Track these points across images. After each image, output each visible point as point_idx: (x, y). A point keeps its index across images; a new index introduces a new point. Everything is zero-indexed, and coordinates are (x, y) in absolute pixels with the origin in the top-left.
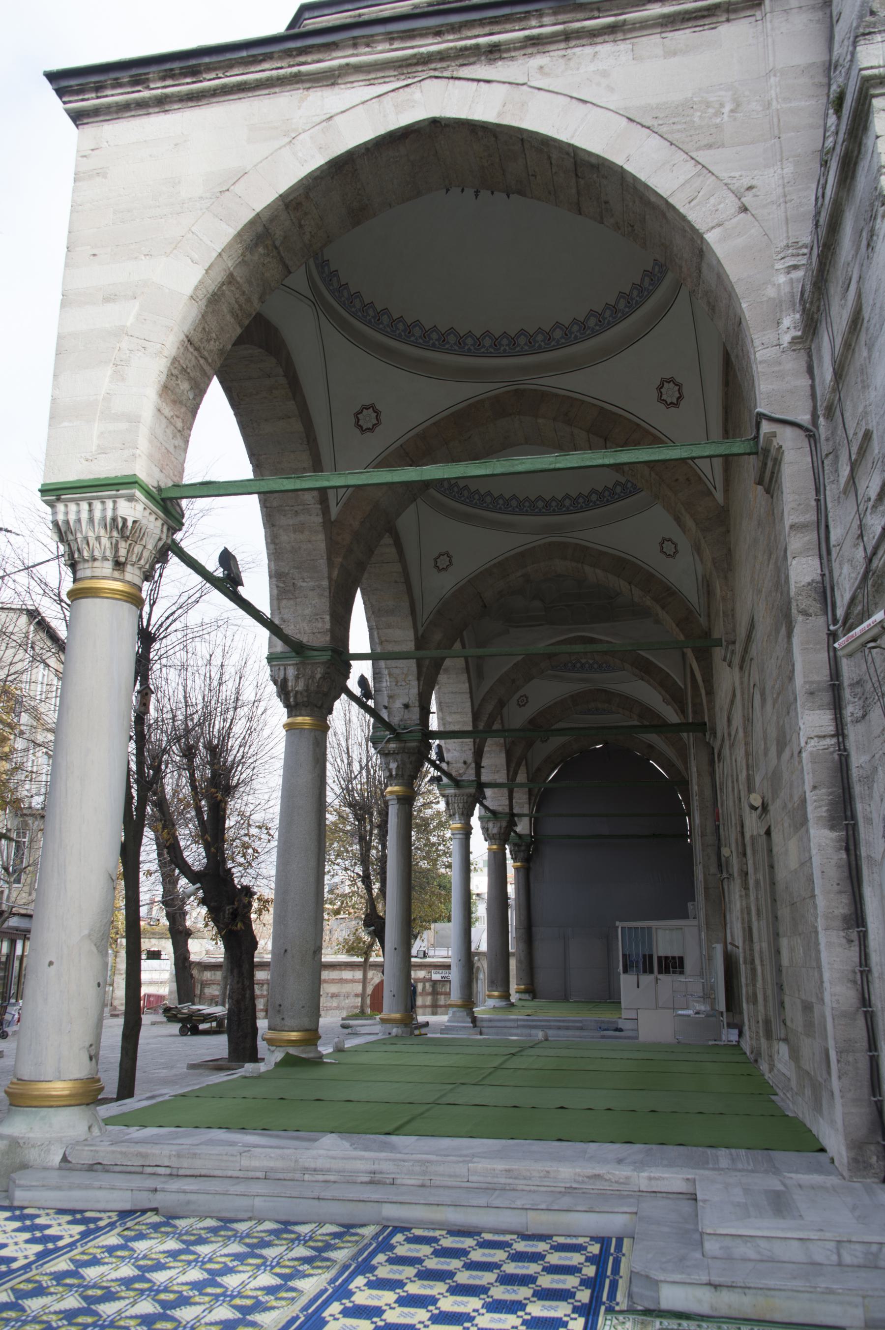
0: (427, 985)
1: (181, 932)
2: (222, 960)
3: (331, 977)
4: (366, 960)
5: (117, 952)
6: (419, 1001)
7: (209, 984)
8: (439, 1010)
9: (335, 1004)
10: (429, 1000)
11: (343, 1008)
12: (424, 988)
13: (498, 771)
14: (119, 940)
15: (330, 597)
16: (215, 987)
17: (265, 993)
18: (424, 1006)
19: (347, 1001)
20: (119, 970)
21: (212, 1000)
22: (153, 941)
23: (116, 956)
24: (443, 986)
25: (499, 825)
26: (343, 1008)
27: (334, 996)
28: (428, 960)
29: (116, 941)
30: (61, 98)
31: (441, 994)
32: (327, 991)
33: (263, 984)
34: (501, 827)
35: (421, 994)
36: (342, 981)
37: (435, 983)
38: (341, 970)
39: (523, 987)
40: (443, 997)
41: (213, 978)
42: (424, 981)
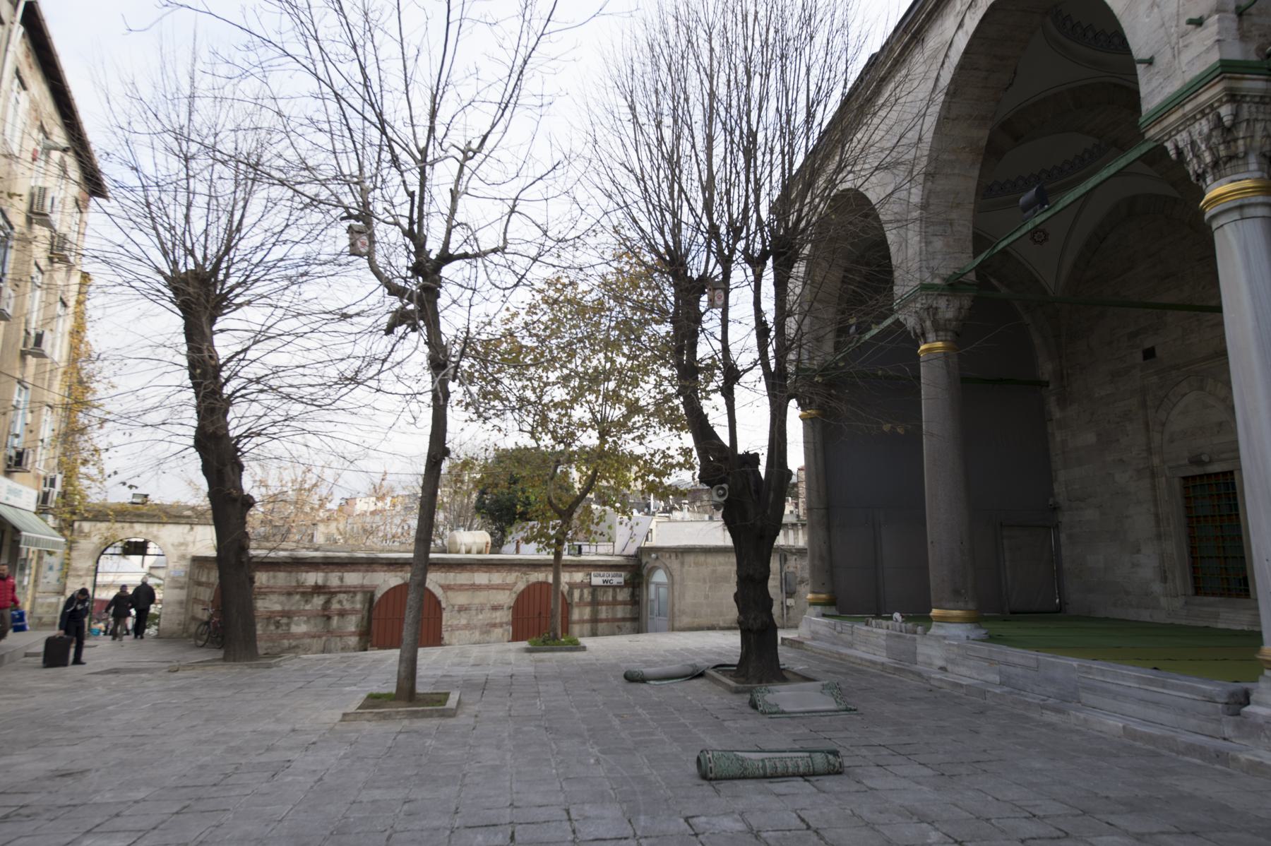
0: (586, 591)
1: (235, 500)
2: (411, 555)
3: (459, 582)
4: (558, 555)
5: (72, 542)
6: (576, 615)
7: (265, 594)
8: (601, 626)
9: (464, 622)
10: (587, 612)
11: (475, 627)
12: (581, 596)
13: (958, 205)
14: (76, 525)
15: (104, 506)
16: (274, 598)
17: (358, 606)
18: (582, 621)
19: (480, 617)
20: (76, 569)
21: (269, 618)
22: (138, 527)
23: (71, 549)
24: (605, 592)
25: (957, 303)
26: (475, 627)
27: (462, 609)
28: (583, 558)
29: (72, 525)
30: (65, 665)
31: (602, 604)
32: (453, 602)
33: (355, 593)
34: (960, 309)
35: (578, 605)
36: (475, 588)
37: (595, 588)
38: (472, 571)
39: (823, 596)
40: (604, 608)
41: (272, 582)
42: (581, 586)
